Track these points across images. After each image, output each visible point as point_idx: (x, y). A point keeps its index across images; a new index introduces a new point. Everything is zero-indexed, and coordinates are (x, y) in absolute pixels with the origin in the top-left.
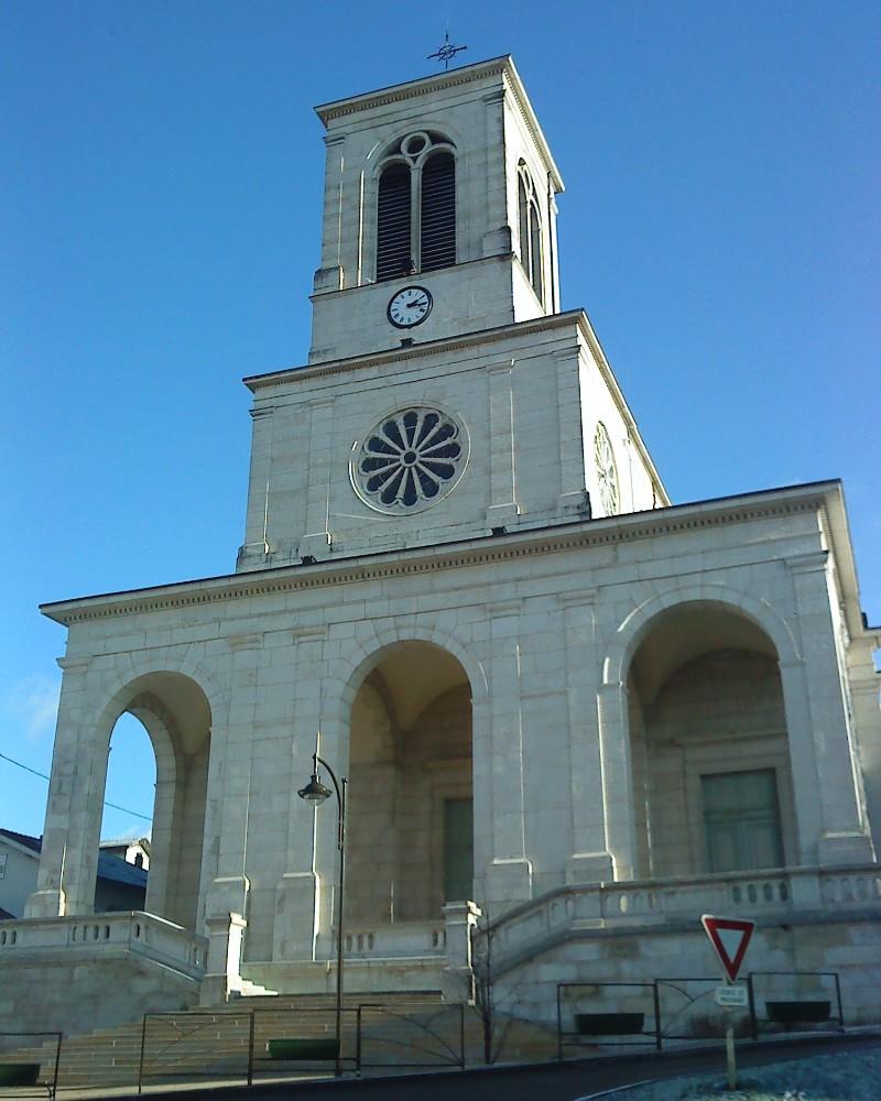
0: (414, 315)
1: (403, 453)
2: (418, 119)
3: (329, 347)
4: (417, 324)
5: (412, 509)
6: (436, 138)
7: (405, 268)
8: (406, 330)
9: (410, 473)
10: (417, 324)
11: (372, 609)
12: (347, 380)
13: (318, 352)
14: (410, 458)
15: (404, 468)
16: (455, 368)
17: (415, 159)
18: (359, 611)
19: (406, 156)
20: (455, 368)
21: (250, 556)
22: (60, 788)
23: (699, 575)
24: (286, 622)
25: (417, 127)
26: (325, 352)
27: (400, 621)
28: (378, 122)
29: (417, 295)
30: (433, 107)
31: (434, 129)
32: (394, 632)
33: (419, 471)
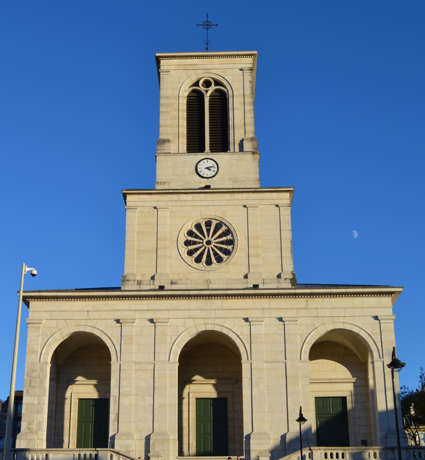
0: (210, 174)
1: (207, 239)
2: (208, 71)
3: (166, 181)
4: (207, 178)
5: (209, 267)
6: (217, 83)
7: (202, 150)
8: (206, 179)
9: (204, 250)
10: (207, 178)
11: (193, 314)
12: (176, 199)
13: (161, 182)
14: (209, 243)
15: (203, 245)
16: (231, 203)
17: (207, 91)
18: (186, 314)
19: (202, 88)
20: (231, 203)
21: (128, 280)
22: (30, 384)
23: (343, 318)
24: (143, 287)
25: (208, 75)
26: (164, 183)
27: (206, 321)
28: (187, 67)
29: (211, 163)
30: (216, 66)
31: (215, 77)
32: (204, 326)
33: (213, 250)
